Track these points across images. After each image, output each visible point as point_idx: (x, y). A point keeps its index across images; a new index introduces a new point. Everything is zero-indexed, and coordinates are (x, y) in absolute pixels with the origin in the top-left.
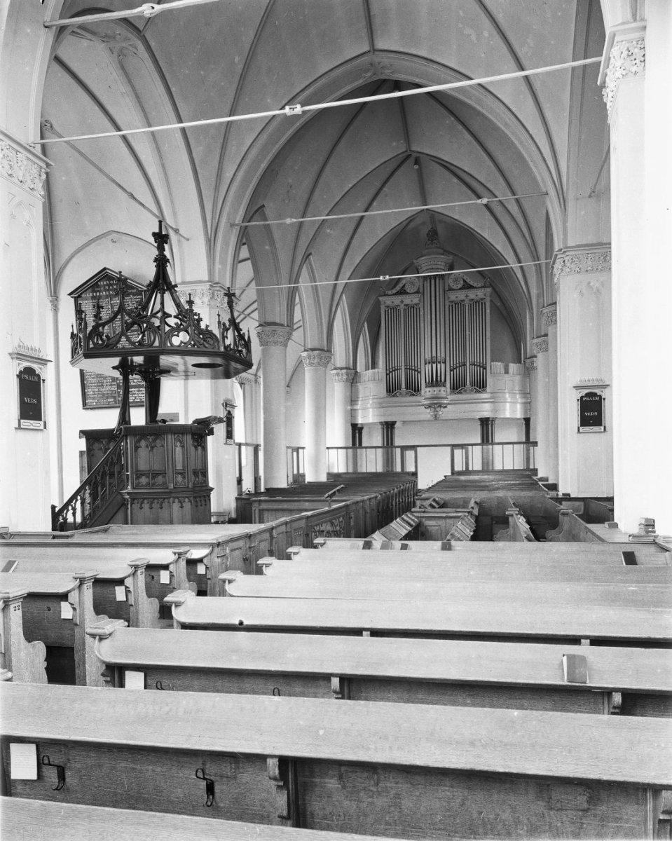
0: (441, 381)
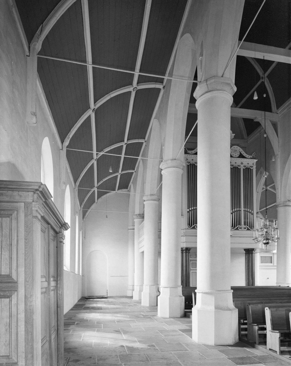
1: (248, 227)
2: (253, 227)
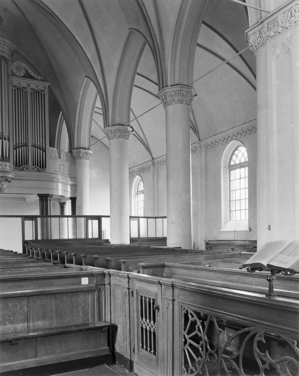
0: (6, 156)
1: (39, 168)
2: (46, 167)
